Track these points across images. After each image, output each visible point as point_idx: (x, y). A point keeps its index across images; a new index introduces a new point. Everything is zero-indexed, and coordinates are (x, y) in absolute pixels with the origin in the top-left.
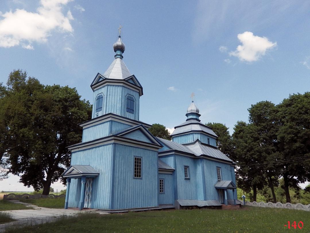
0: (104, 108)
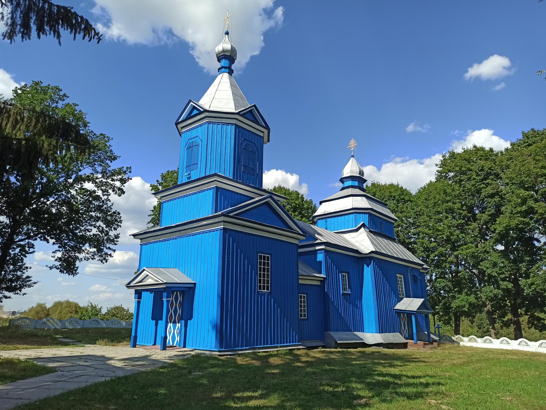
0: (201, 165)
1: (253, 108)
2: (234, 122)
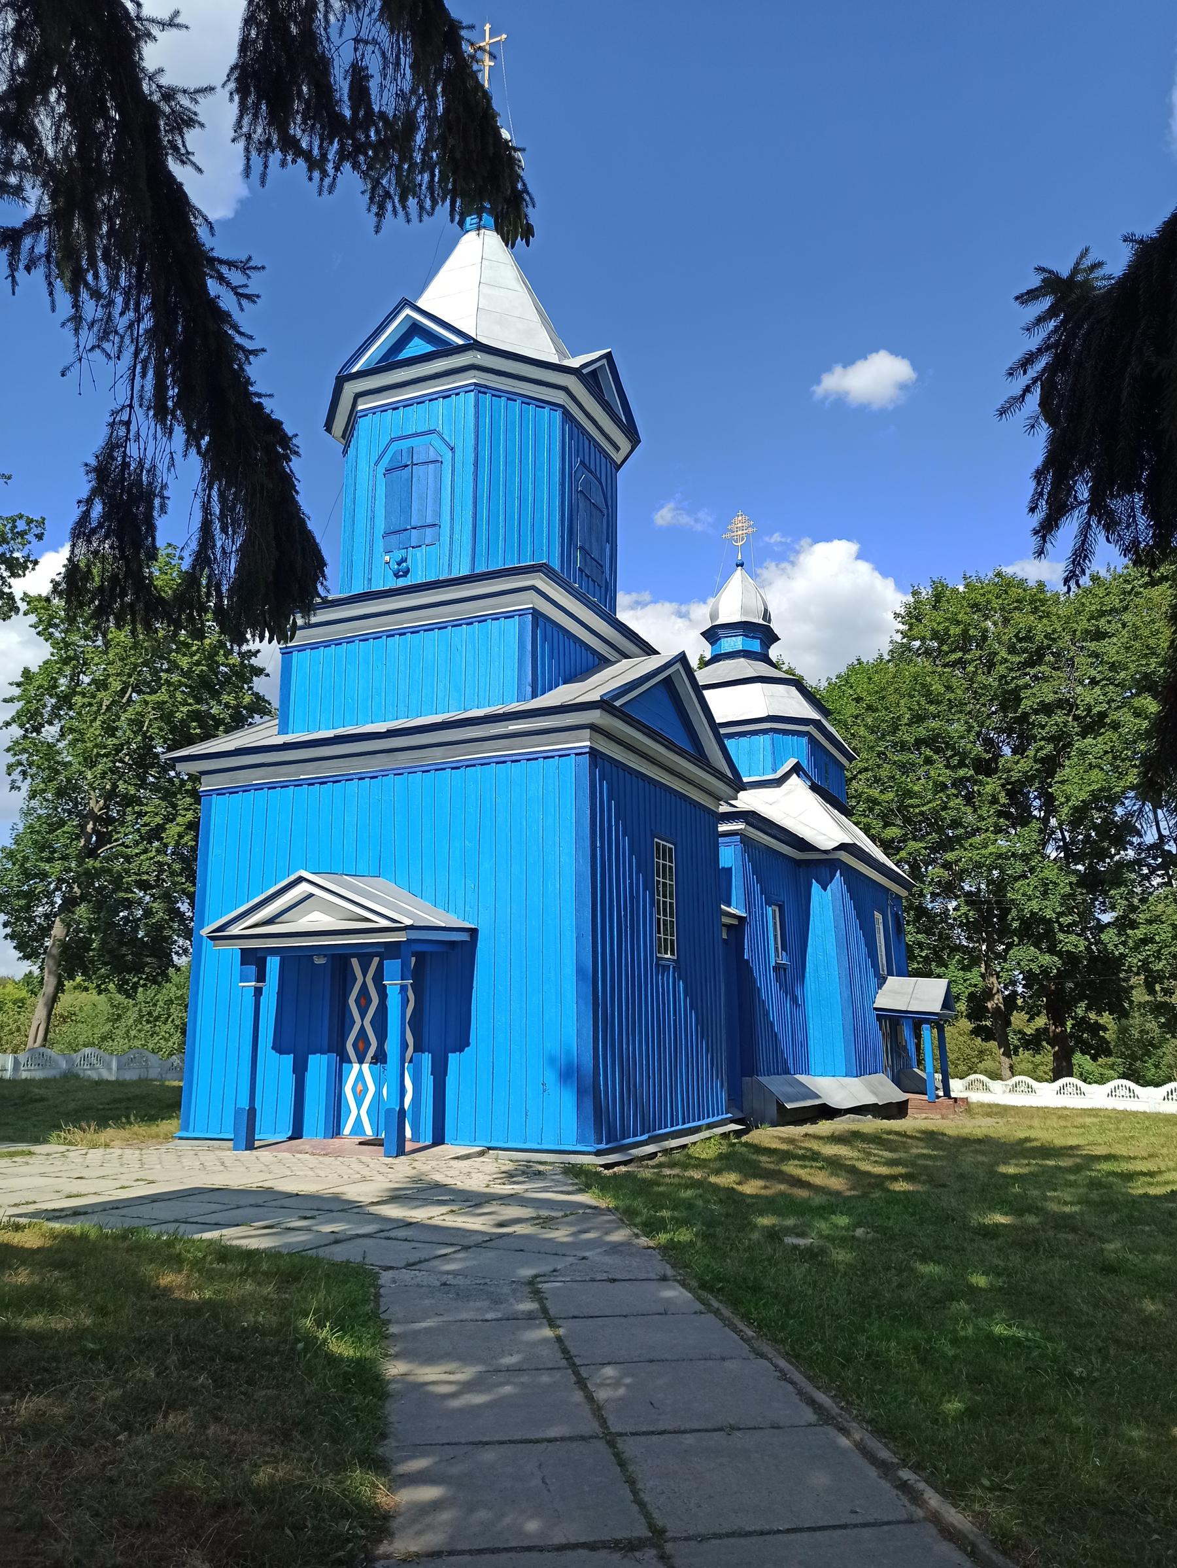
2: (559, 397)
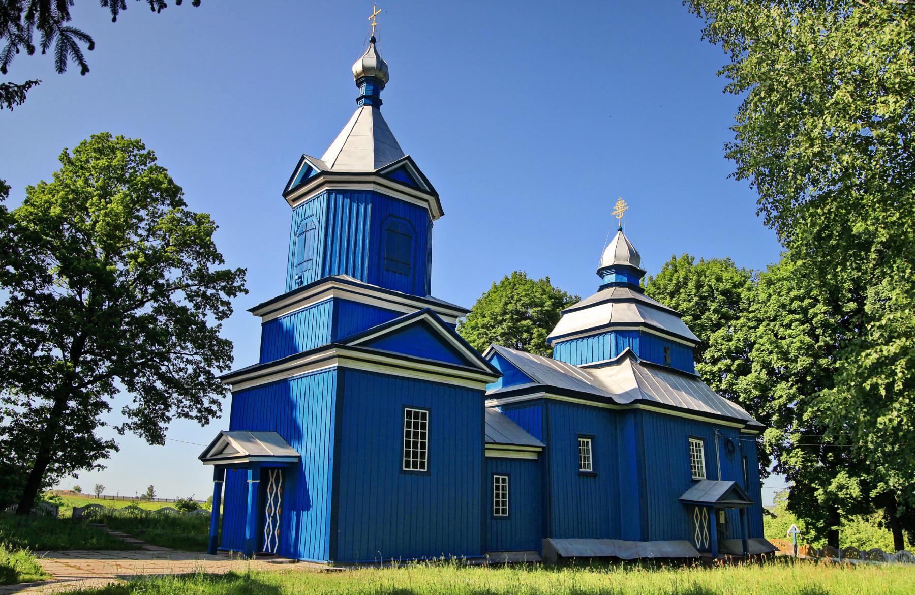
1: (407, 161)
